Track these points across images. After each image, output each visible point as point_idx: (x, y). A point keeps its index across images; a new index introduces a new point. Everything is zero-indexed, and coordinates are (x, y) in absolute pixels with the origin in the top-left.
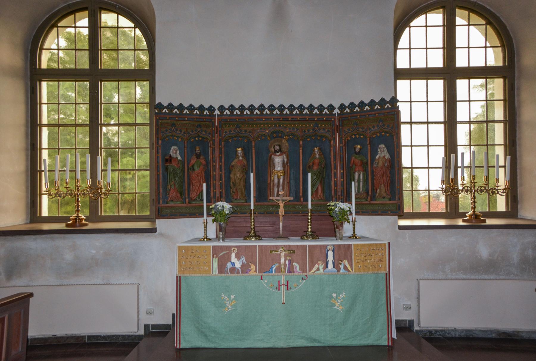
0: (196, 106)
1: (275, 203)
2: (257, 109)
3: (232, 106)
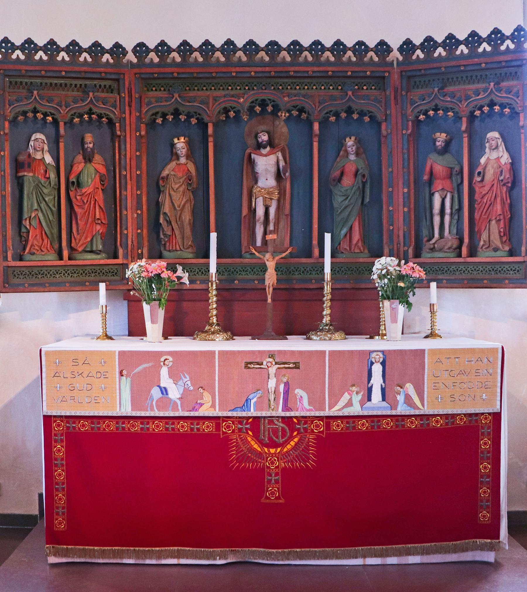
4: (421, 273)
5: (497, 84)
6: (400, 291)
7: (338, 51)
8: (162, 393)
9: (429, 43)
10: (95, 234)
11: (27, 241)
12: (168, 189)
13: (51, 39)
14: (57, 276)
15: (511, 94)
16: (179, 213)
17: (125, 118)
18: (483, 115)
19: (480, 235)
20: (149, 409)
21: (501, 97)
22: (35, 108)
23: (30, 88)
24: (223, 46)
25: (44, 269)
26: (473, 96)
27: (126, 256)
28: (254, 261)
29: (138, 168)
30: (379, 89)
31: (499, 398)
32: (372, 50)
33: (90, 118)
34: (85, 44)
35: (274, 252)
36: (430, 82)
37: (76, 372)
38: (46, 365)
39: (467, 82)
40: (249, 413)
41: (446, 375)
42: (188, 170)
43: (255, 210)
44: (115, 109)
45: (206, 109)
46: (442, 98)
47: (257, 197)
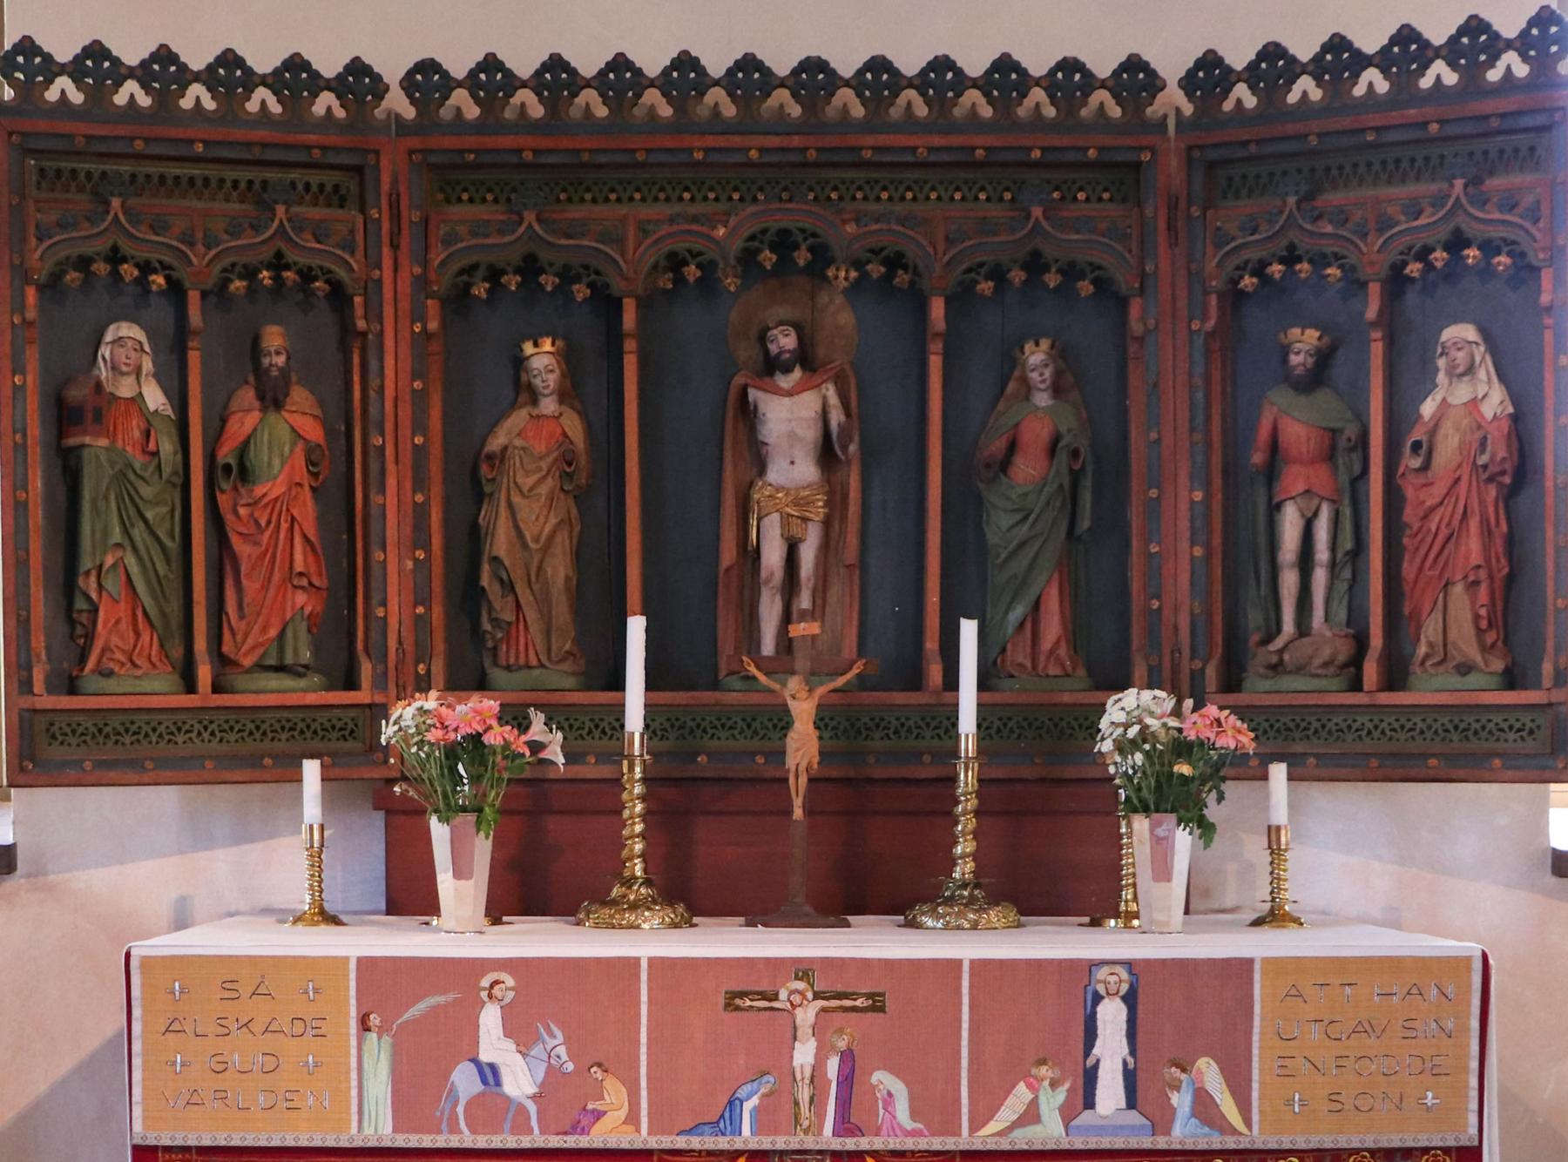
2: (197, 77)
5: (1475, 181)
8: (485, 1082)
9: (1273, 64)
10: (292, 618)
11: (90, 636)
13: (163, 47)
14: (180, 739)
17: (380, 281)
19: (1419, 627)
21: (1485, 220)
22: (115, 249)
24: (666, 72)
25: (140, 719)
26: (1403, 218)
27: (380, 682)
28: (754, 698)
29: (419, 426)
30: (1124, 200)
31: (1474, 1105)
32: (1103, 84)
33: (277, 278)
34: (264, 60)
35: (813, 674)
37: (232, 1019)
40: (737, 1139)
41: (1315, 1033)
42: (564, 434)
43: (758, 550)
44: (352, 254)
45: (618, 257)
46: (1308, 227)
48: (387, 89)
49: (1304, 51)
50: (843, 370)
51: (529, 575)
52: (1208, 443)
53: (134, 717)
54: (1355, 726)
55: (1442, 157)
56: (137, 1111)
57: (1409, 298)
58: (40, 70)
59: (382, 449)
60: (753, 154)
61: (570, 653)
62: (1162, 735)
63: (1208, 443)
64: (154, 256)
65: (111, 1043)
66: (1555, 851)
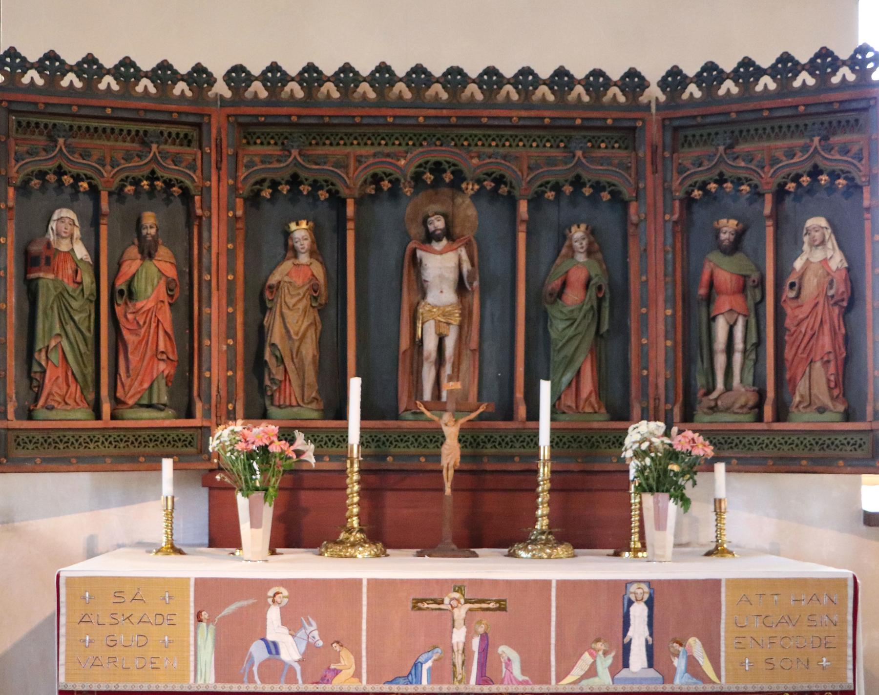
0: (109, 62)
1: (428, 425)
3: (274, 68)
4: (706, 449)
5: (825, 138)
6: (667, 477)
7: (561, 85)
8: (270, 652)
9: (711, 74)
10: (157, 377)
11: (41, 387)
12: (278, 306)
13: (90, 54)
14: (92, 446)
15: (849, 154)
16: (297, 344)
17: (210, 188)
18: (799, 190)
19: (795, 387)
20: (245, 679)
21: (833, 160)
22: (60, 167)
23: (52, 133)
24: (373, 74)
25: (69, 434)
26: (784, 159)
27: (207, 414)
28: (421, 425)
29: (231, 269)
30: (626, 148)
31: (850, 666)
32: (615, 84)
33: (152, 186)
34: (146, 64)
35: (457, 411)
36: (711, 137)
37: (120, 614)
38: (67, 602)
39: (773, 135)
40: (419, 686)
41: (757, 623)
42: (313, 275)
43: (422, 341)
44: (195, 172)
45: (344, 176)
46: (731, 163)
47: (425, 320)
48: (215, 81)
49: (728, 66)
50: (470, 241)
51: (292, 355)
52: (674, 282)
53: (65, 433)
54: (759, 442)
55: (806, 125)
56: (62, 670)
57: (787, 201)
58: (19, 66)
59: (209, 282)
60: (421, 120)
61: (315, 398)
62: (661, 448)
63: (674, 282)
64: (82, 172)
65: (48, 620)
66: (865, 512)
